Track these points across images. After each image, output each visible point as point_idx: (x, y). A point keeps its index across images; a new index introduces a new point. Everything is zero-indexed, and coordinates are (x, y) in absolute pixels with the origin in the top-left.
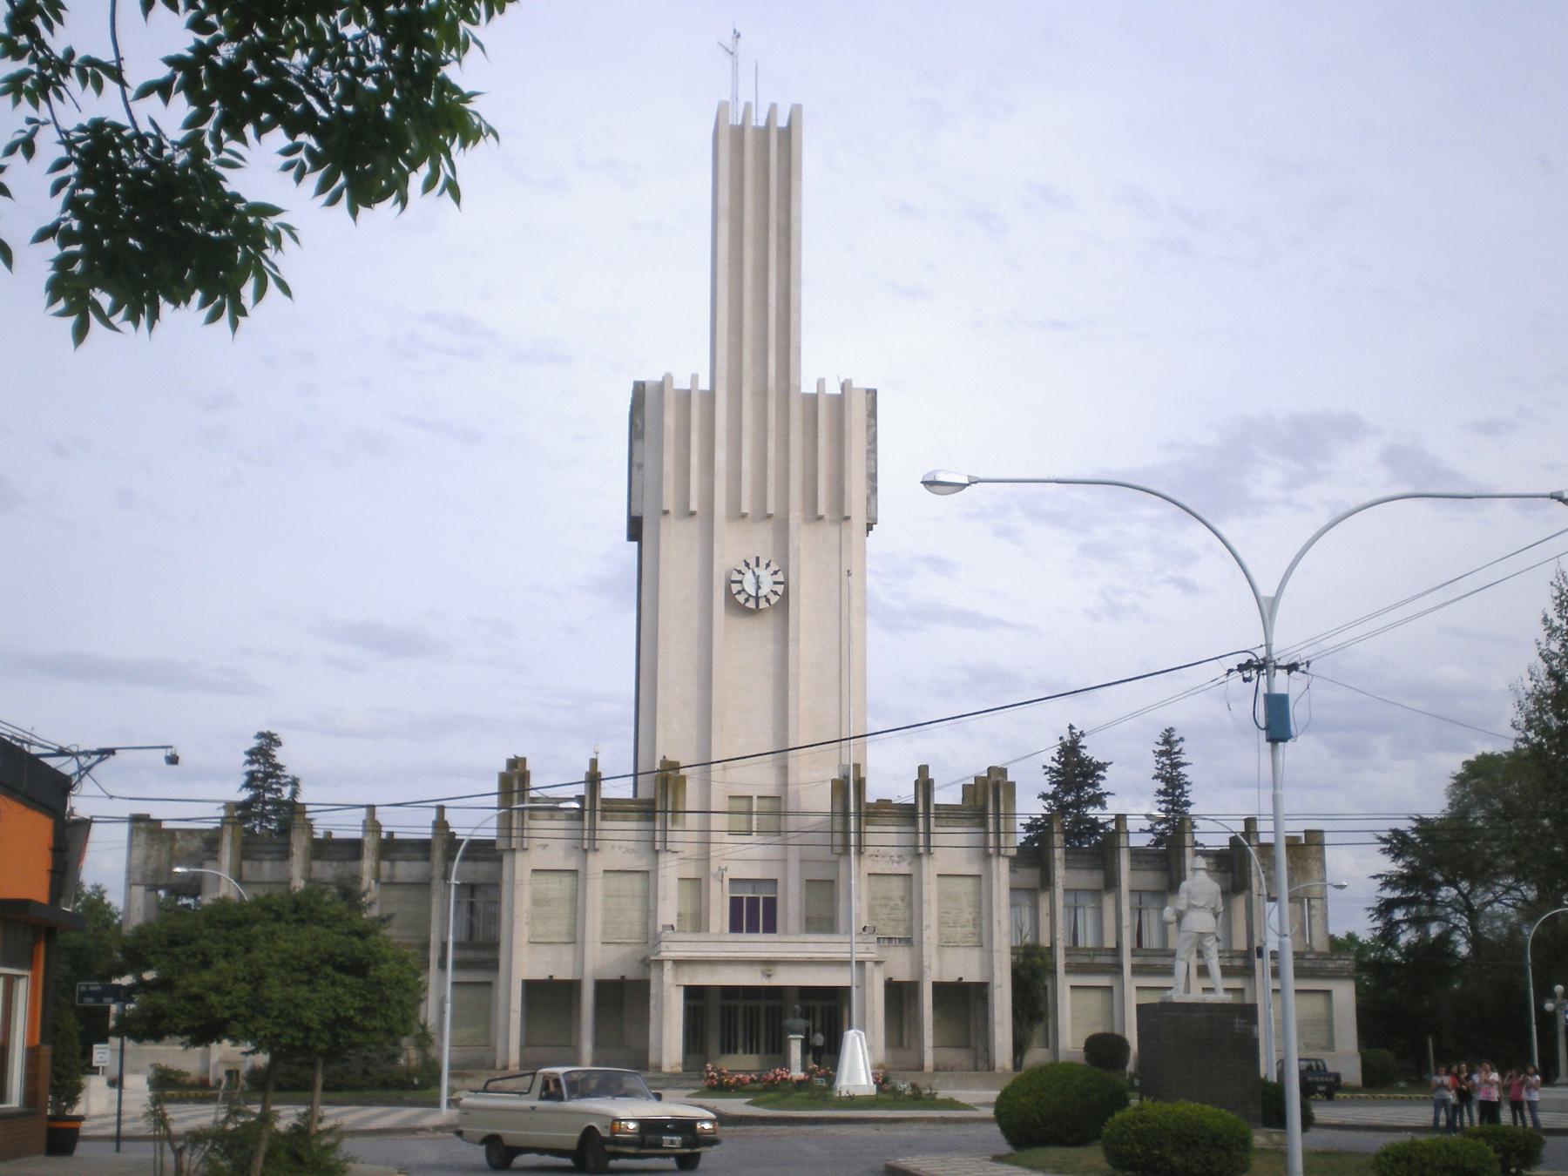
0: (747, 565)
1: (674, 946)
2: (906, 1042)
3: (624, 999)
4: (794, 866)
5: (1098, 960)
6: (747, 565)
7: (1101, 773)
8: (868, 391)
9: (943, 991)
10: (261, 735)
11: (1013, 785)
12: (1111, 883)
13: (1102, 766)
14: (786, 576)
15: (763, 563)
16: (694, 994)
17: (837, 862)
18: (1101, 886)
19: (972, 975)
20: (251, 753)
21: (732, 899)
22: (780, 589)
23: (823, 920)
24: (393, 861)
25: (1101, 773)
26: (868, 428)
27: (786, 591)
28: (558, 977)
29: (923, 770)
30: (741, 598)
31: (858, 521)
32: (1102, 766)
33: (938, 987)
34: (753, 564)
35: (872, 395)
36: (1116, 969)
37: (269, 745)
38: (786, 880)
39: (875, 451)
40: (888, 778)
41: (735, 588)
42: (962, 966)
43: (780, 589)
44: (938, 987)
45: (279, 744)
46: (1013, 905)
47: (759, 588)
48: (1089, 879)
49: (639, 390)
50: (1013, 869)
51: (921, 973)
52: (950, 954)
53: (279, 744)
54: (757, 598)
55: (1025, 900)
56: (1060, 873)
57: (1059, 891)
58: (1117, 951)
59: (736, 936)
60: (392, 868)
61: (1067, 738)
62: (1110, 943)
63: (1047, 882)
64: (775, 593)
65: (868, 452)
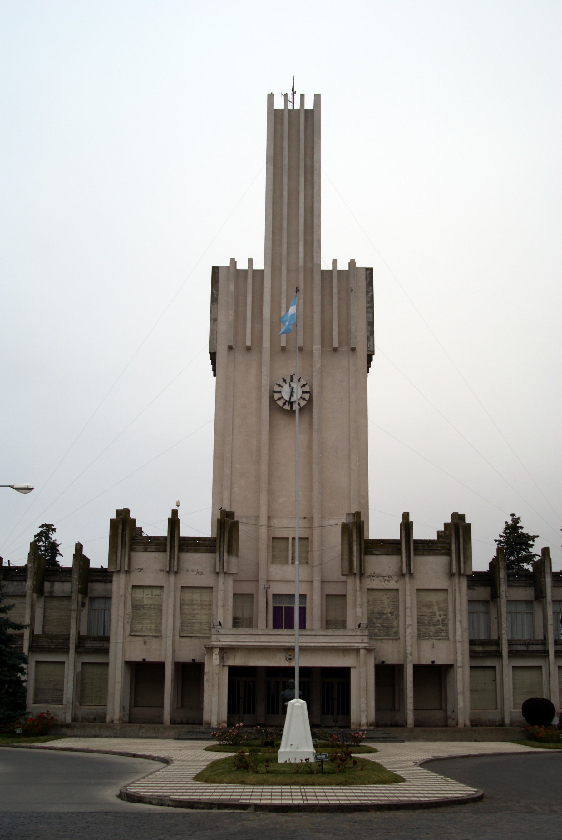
0: (285, 381)
1: (221, 638)
2: (397, 707)
3: (191, 675)
4: (317, 585)
5: (531, 648)
6: (285, 381)
7: (531, 542)
8: (367, 269)
9: (420, 670)
10: (43, 526)
11: (469, 526)
12: (540, 595)
13: (533, 538)
14: (311, 387)
15: (295, 379)
16: (235, 673)
17: (346, 582)
18: (533, 599)
19: (441, 660)
20: (38, 535)
21: (275, 609)
22: (307, 396)
23: (334, 622)
24: (52, 582)
25: (531, 542)
26: (367, 292)
27: (311, 398)
28: (148, 659)
29: (406, 516)
30: (280, 403)
31: (362, 353)
32: (533, 538)
33: (417, 668)
34: (288, 380)
35: (369, 272)
36: (545, 654)
37: (48, 531)
38: (312, 595)
39: (372, 307)
40: (382, 526)
41: (276, 396)
42: (434, 653)
43: (307, 396)
44: (417, 668)
45: (54, 530)
46: (470, 613)
47: (292, 395)
48: (524, 593)
49: (215, 271)
50: (469, 587)
51: (406, 657)
52: (426, 645)
53: (54, 530)
54: (291, 403)
55: (480, 608)
56: (503, 588)
57: (503, 601)
58: (544, 642)
59: (279, 631)
60: (52, 587)
61: (510, 522)
62: (540, 636)
63: (495, 595)
64: (304, 399)
65: (367, 308)
